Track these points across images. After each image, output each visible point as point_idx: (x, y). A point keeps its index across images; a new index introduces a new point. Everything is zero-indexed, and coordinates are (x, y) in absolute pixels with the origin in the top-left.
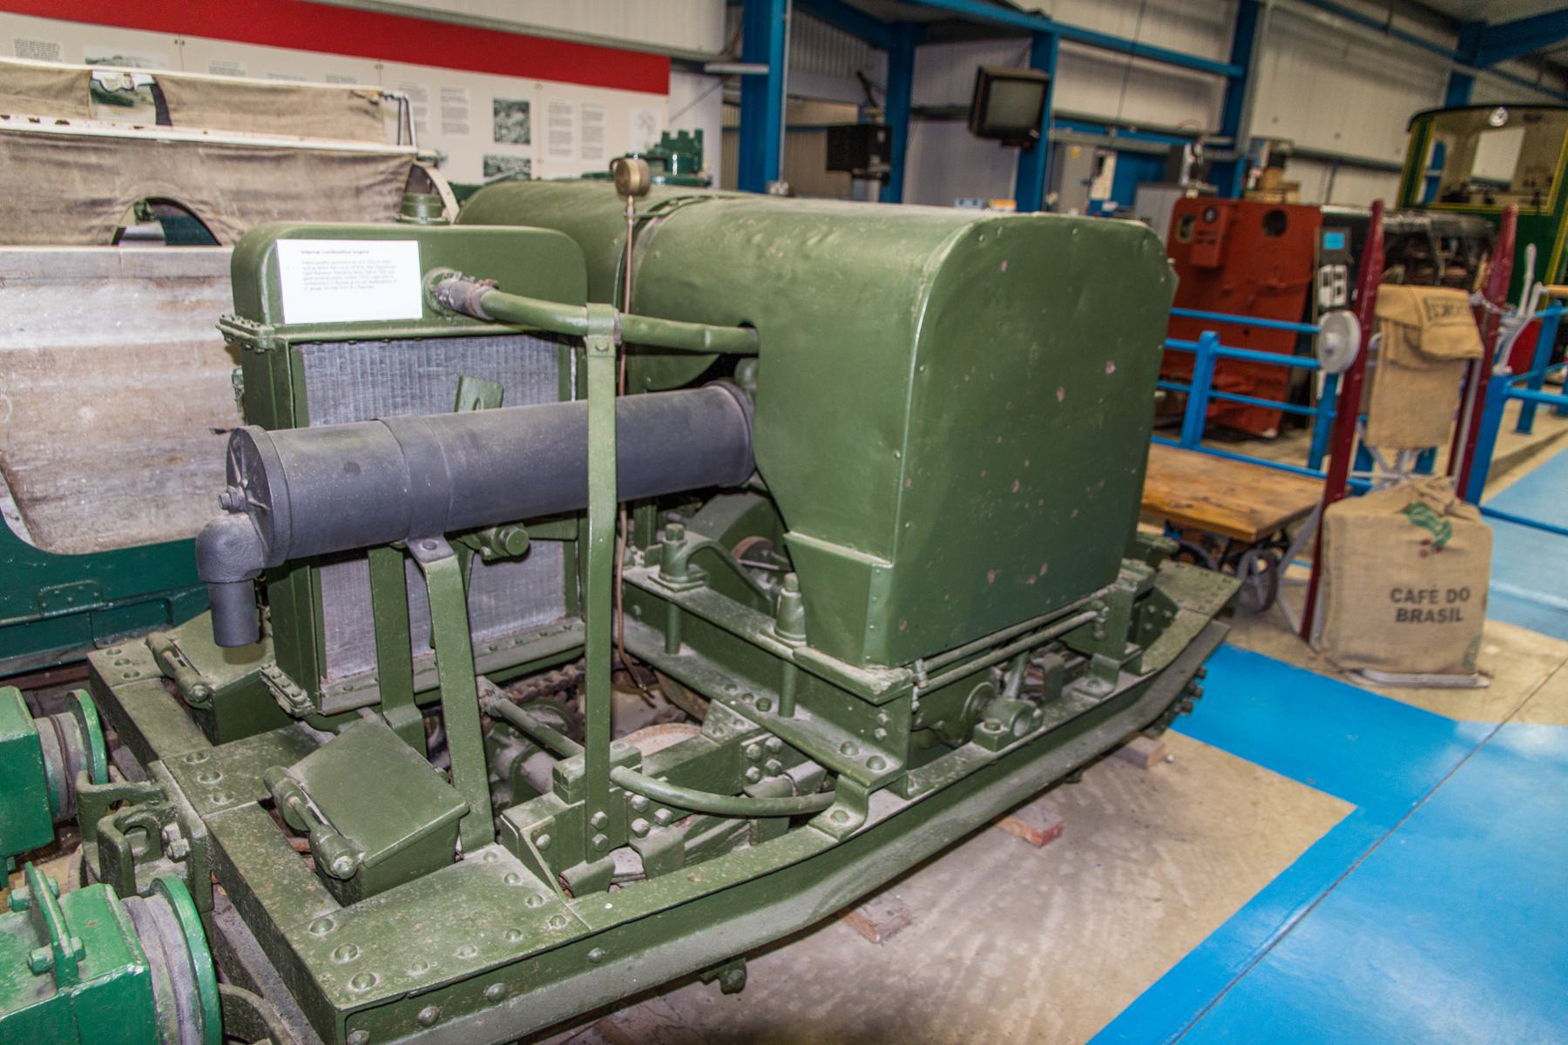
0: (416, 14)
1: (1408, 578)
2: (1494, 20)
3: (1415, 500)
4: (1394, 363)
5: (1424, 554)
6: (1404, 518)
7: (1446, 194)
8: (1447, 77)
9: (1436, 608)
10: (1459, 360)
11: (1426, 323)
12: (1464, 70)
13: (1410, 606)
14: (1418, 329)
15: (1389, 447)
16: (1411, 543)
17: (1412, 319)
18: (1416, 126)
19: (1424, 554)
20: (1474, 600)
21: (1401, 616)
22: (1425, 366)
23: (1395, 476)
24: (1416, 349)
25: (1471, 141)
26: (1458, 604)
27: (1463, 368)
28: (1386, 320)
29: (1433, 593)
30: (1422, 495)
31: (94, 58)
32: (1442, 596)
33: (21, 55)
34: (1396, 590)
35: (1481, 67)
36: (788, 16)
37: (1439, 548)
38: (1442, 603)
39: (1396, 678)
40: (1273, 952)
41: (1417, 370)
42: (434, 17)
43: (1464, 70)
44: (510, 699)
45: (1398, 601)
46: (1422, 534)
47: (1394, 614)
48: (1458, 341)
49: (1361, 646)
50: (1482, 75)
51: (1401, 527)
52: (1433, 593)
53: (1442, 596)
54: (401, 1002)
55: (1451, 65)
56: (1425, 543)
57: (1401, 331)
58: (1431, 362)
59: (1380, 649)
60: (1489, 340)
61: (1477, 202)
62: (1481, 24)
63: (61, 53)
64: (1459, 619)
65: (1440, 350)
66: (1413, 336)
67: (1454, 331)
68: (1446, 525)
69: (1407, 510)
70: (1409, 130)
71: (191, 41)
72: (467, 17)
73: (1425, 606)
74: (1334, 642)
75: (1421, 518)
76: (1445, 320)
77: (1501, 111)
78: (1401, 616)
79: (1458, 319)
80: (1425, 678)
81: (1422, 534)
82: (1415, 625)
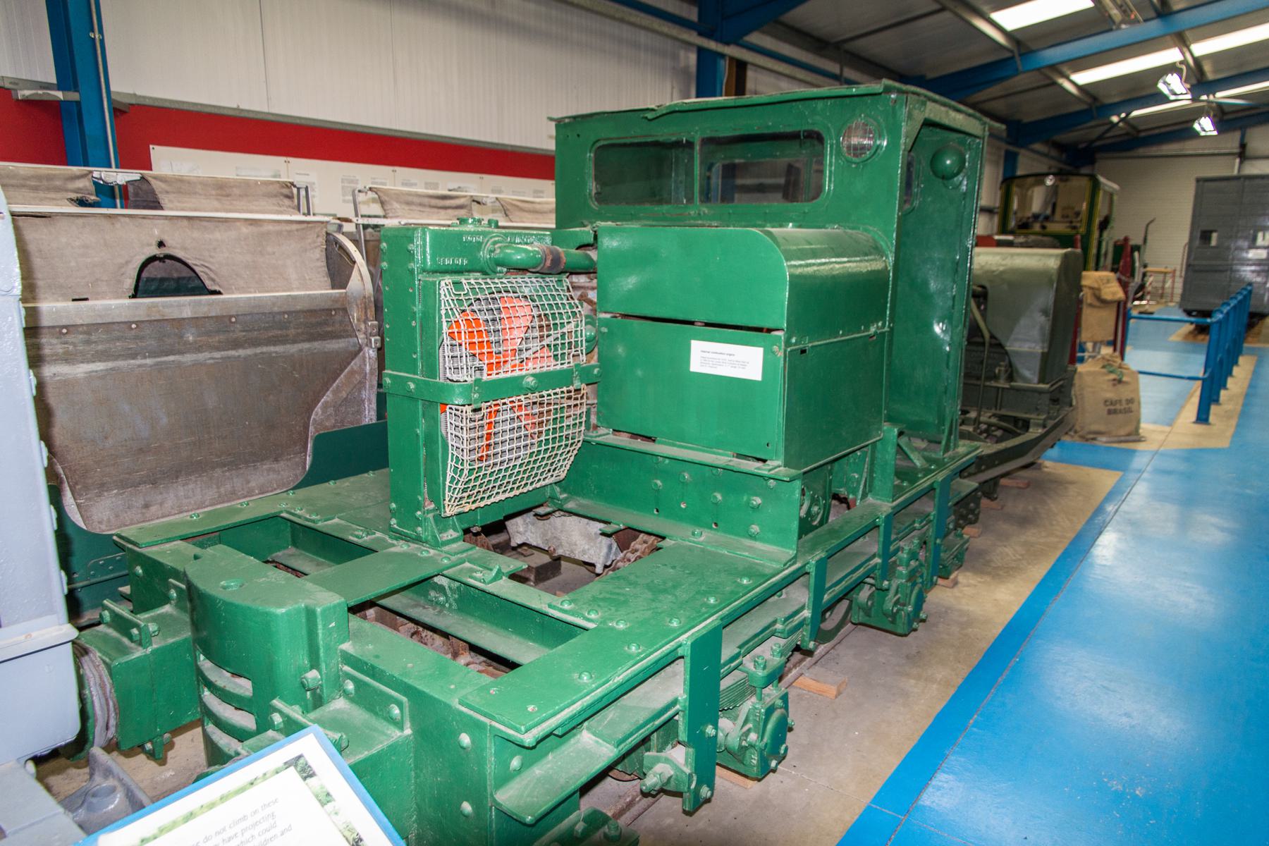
0: (367, 131)
1: (1110, 395)
2: (1026, 120)
3: (1106, 363)
4: (1091, 305)
5: (1114, 385)
6: (1104, 370)
7: (1020, 223)
8: (1003, 153)
9: (1122, 407)
10: (1115, 302)
11: (1102, 287)
12: (1011, 148)
13: (1112, 407)
14: (1099, 289)
15: (1090, 342)
16: (1109, 380)
17: (1096, 285)
18: (1004, 186)
19: (1114, 385)
20: (1136, 403)
21: (1110, 412)
22: (1102, 305)
23: (1094, 354)
24: (1099, 299)
25: (1030, 192)
26: (1130, 405)
27: (1115, 305)
28: (1086, 286)
29: (1120, 401)
30: (1108, 360)
31: (451, 188)
32: (1124, 402)
33: (426, 188)
34: (1106, 401)
35: (1022, 147)
36: (834, 160)
37: (1120, 381)
38: (1124, 406)
39: (1112, 439)
40: (1120, 509)
41: (1099, 307)
42: (185, 107)
43: (1011, 148)
44: (514, 577)
45: (1107, 406)
46: (1112, 376)
47: (1106, 412)
48: (1114, 294)
49: (1094, 427)
50: (1023, 151)
51: (1105, 374)
52: (1120, 401)
53: (1124, 402)
54: (525, 750)
55: (1005, 146)
56: (1114, 380)
57: (1091, 291)
58: (1104, 303)
59: (1102, 428)
60: (1126, 293)
61: (1037, 227)
62: (1019, 122)
63: (440, 187)
64: (1131, 412)
65: (1108, 297)
66: (1097, 292)
67: (1111, 289)
68: (1121, 372)
69: (1104, 367)
70: (1001, 188)
71: (398, 169)
72: (401, 131)
73: (1118, 407)
74: (1082, 428)
75: (1111, 369)
76: (1109, 285)
77: (1051, 177)
78: (1110, 412)
79: (1113, 284)
80: (1123, 438)
81: (1112, 376)
82: (1114, 416)
